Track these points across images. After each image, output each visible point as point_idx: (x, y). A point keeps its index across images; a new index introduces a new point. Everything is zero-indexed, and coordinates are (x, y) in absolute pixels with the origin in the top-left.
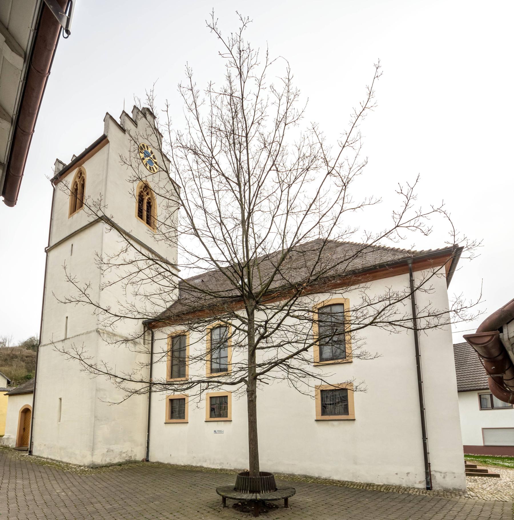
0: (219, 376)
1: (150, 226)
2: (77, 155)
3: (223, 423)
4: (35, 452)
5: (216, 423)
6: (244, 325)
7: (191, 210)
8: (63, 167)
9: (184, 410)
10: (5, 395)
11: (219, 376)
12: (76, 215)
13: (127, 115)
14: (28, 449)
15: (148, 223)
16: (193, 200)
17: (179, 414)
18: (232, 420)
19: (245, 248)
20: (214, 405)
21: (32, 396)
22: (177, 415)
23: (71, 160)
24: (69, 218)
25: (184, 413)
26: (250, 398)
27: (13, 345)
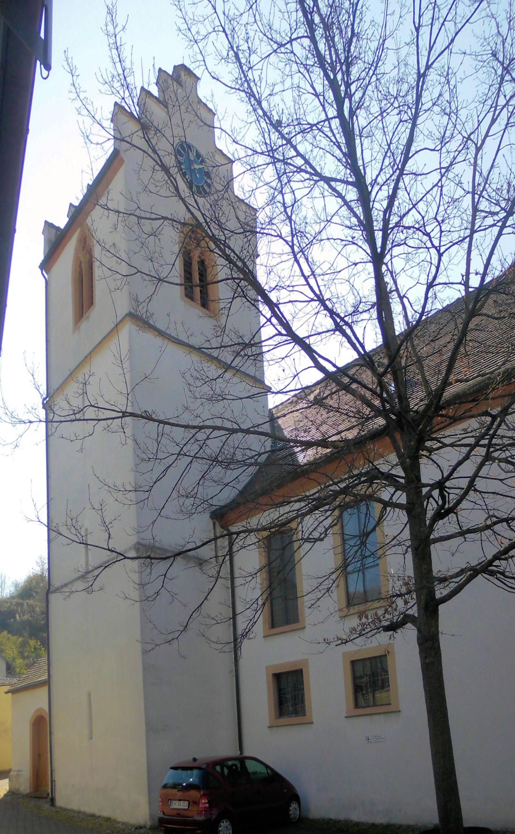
0: (461, 580)
1: (208, 310)
2: (76, 203)
3: (382, 717)
4: (60, 802)
5: (368, 718)
6: (399, 493)
7: (476, 20)
8: (56, 234)
9: (303, 695)
10: (6, 693)
11: (461, 580)
12: (84, 325)
13: (149, 93)
14: (48, 794)
15: (205, 304)
16: (226, 304)
17: (295, 705)
18: (400, 709)
19: (355, 341)
20: (361, 677)
21: (46, 688)
22: (291, 709)
23: (68, 216)
24: (74, 333)
25: (303, 701)
26: (426, 658)
27: (31, 571)
